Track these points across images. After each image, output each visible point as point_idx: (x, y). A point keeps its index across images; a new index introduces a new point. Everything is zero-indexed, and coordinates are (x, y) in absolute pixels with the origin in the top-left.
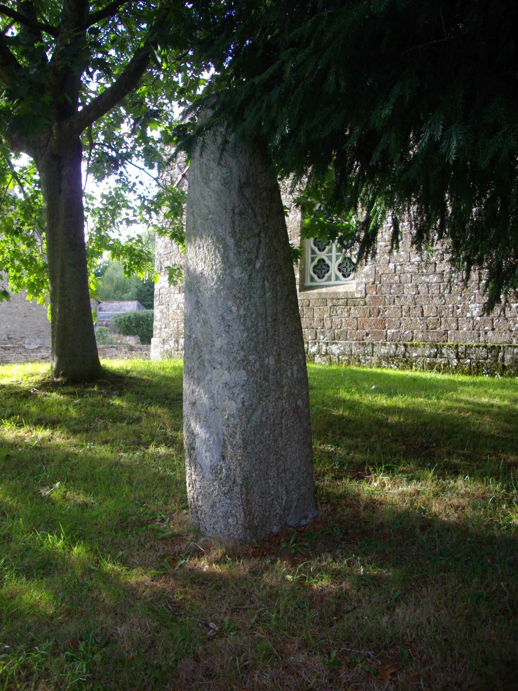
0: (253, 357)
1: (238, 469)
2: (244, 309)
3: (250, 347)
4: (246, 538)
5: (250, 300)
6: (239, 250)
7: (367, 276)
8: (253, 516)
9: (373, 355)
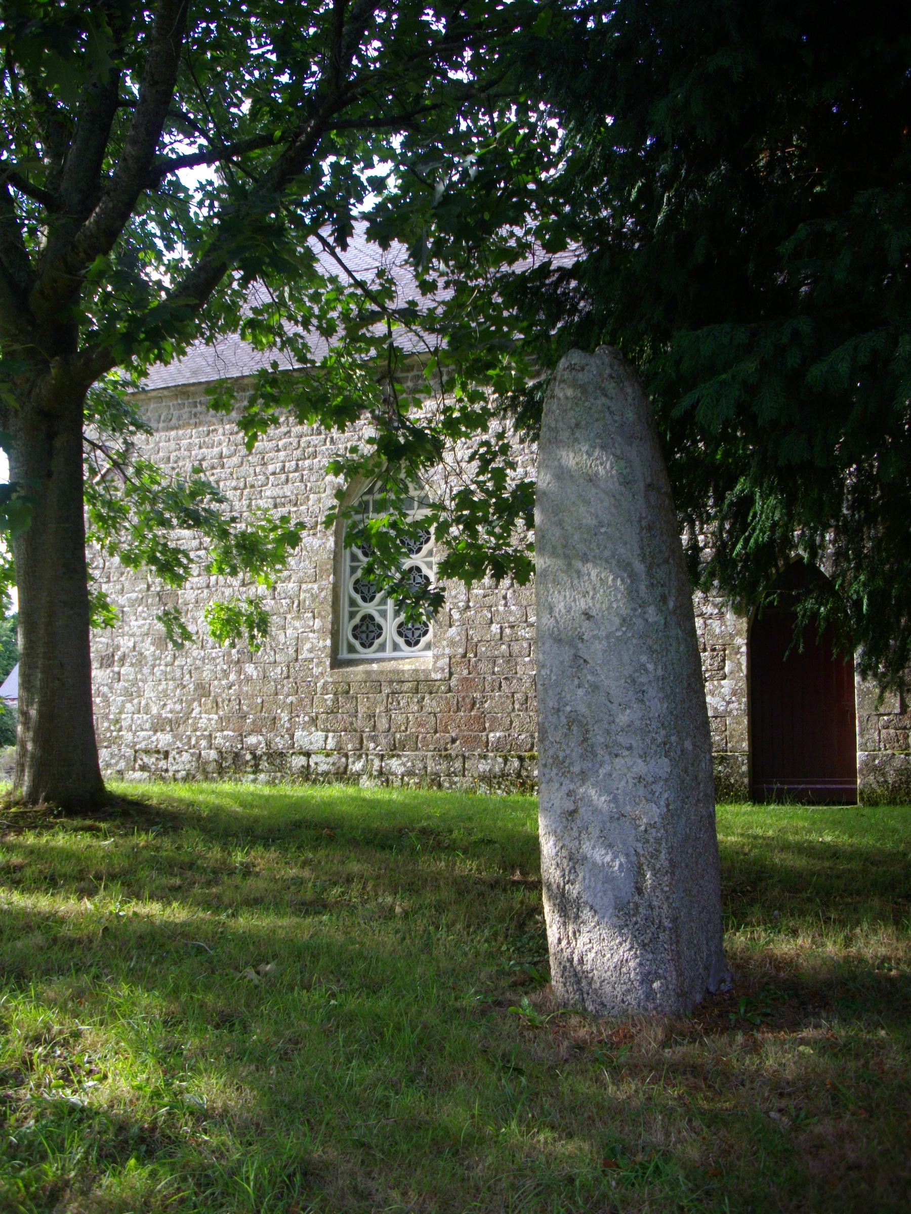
1: (665, 906)
7: (452, 643)
9: (464, 776)
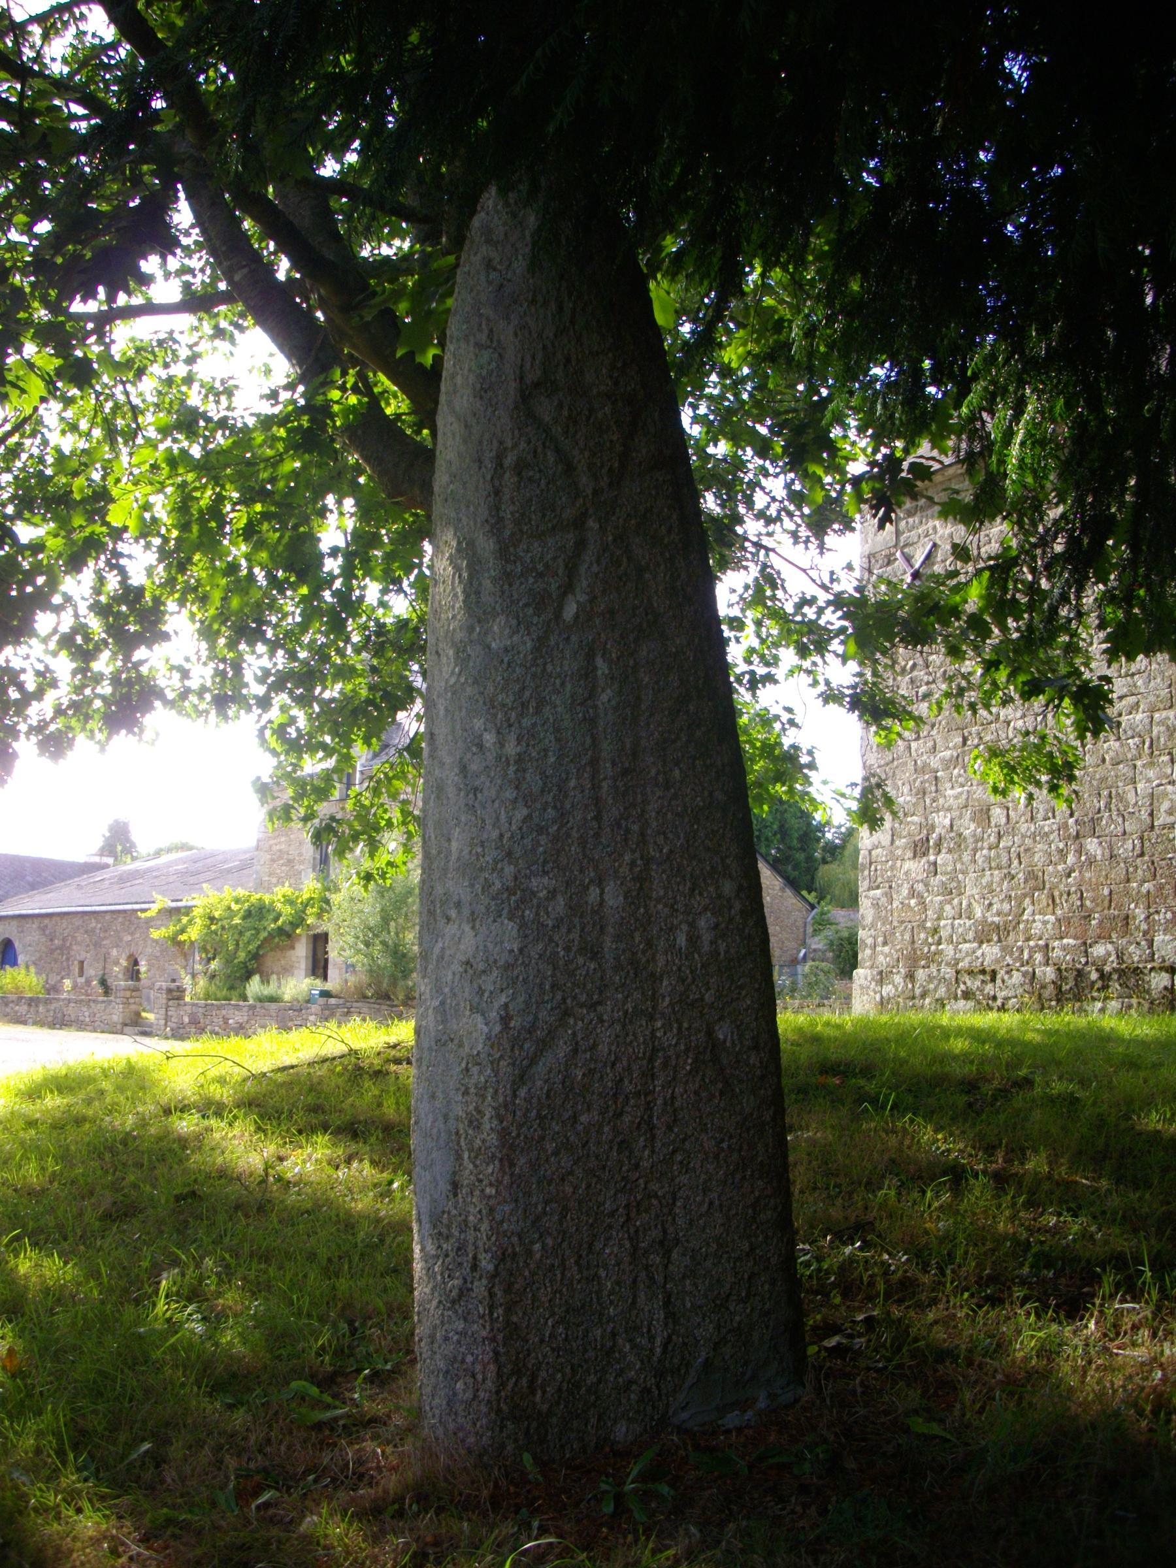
0: (546, 880)
1: (484, 1226)
2: (519, 740)
3: (534, 850)
4: (503, 1446)
5: (538, 711)
6: (509, 568)
8: (533, 1378)
